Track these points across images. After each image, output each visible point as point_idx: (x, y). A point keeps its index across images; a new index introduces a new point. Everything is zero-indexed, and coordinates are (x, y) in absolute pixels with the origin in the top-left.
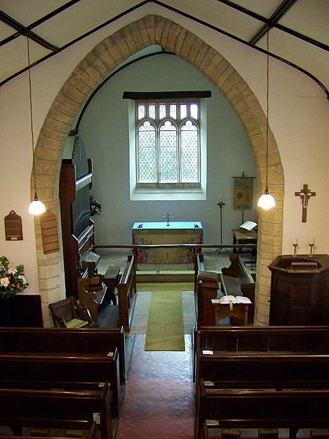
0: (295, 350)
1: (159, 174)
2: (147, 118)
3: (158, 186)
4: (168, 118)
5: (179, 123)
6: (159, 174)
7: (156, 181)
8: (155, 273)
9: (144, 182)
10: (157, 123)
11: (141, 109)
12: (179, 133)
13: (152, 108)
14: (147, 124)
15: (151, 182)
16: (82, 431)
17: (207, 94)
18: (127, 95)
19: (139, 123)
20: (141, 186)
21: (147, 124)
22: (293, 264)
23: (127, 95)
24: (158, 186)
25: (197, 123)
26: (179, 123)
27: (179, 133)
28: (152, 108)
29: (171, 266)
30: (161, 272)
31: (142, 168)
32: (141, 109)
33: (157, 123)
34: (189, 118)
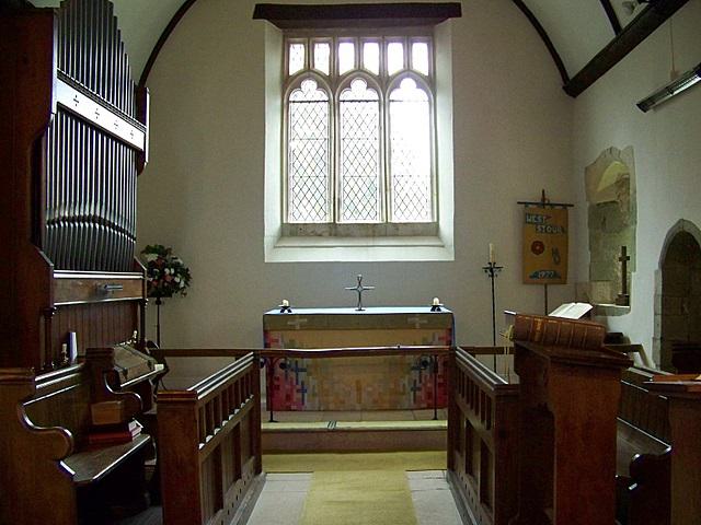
1: (336, 203)
2: (309, 71)
3: (336, 231)
7: (328, 219)
10: (334, 83)
11: (297, 53)
17: (454, 11)
19: (289, 83)
20: (291, 232)
23: (262, 12)
24: (336, 231)
25: (429, 83)
26: (383, 84)
33: (334, 83)
34: (408, 71)
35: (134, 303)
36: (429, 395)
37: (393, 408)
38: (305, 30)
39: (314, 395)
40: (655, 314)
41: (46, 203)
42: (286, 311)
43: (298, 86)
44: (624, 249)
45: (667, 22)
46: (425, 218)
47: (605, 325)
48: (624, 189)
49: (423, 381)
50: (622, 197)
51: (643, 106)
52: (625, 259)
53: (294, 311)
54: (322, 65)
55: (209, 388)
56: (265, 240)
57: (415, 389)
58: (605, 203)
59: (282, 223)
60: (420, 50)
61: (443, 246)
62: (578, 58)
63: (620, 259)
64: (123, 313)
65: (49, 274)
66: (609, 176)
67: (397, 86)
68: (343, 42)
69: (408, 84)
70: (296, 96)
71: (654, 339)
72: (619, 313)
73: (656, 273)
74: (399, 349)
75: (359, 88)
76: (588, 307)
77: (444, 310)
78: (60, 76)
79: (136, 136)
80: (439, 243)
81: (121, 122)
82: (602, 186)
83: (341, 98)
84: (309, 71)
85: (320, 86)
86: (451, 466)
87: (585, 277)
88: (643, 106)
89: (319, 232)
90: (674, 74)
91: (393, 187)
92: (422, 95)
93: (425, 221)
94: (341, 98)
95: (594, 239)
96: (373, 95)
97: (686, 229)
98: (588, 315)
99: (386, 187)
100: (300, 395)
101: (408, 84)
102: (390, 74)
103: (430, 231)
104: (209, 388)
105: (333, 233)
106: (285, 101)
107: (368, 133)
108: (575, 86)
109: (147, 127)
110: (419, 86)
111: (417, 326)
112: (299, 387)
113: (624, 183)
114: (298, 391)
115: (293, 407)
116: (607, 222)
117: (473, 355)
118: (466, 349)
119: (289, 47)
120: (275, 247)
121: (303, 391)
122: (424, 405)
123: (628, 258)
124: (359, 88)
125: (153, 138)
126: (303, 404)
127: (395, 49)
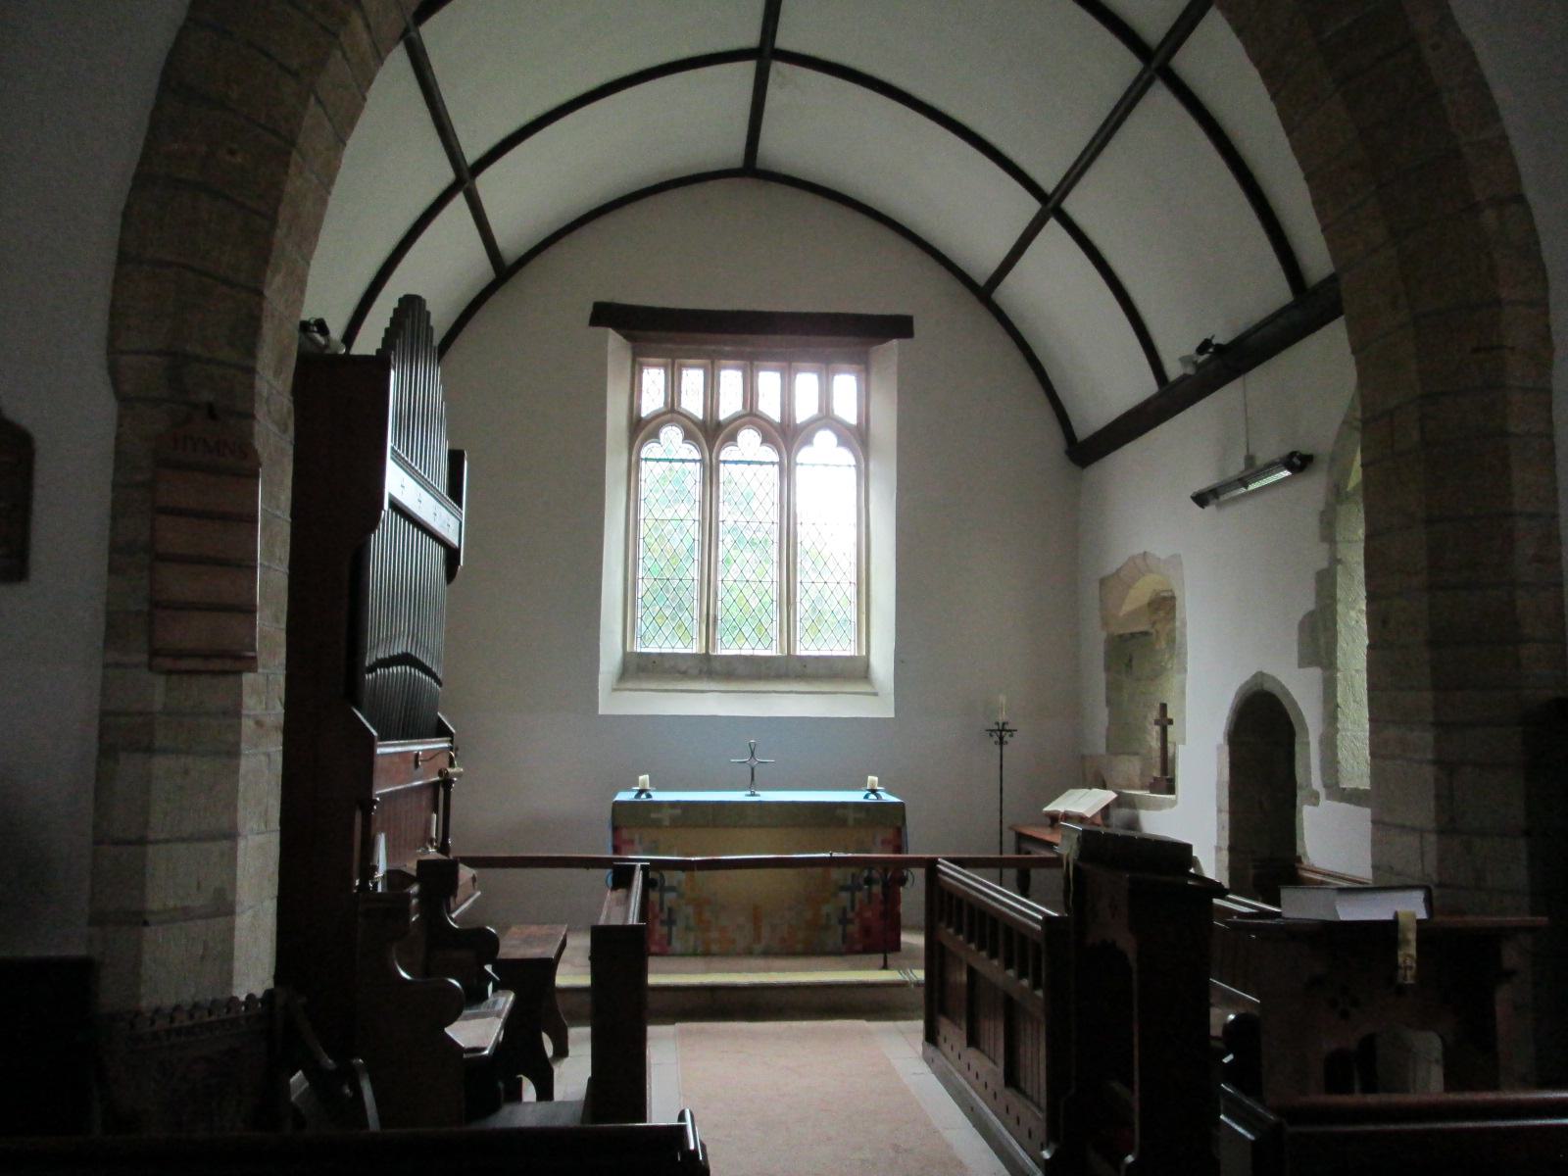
0: (1244, 997)
1: (710, 622)
2: (672, 412)
3: (709, 668)
4: (750, 415)
5: (785, 436)
6: (710, 622)
7: (696, 648)
8: (828, 855)
9: (653, 649)
10: (710, 433)
11: (653, 379)
12: (786, 471)
13: (408, 668)
14: (672, 435)
15: (680, 649)
16: (1343, 918)
17: (899, 327)
18: (606, 315)
19: (641, 429)
20: (642, 668)
21: (672, 435)
22: (1040, 917)
23: (606, 315)
24: (709, 668)
25: (858, 438)
26: (785, 436)
27: (786, 471)
28: (693, 379)
29: (716, 962)
30: (835, 855)
31: (649, 598)
32: (653, 379)
33: (710, 433)
34: (825, 417)
35: (435, 785)
36: (866, 931)
37: (811, 949)
38: (669, 346)
39: (688, 929)
40: (1219, 811)
41: (371, 638)
42: (643, 796)
43: (654, 435)
44: (1164, 707)
45: (1238, 382)
46: (842, 646)
47: (1133, 823)
48: (1162, 614)
49: (857, 907)
50: (1158, 626)
51: (1201, 499)
52: (1164, 722)
53: (658, 796)
54: (692, 402)
55: (981, 883)
56: (600, 677)
57: (844, 921)
58: (1133, 635)
59: (625, 653)
60: (846, 387)
61: (875, 694)
62: (1094, 412)
63: (1157, 723)
64: (425, 800)
65: (370, 744)
66: (1140, 594)
67: (808, 441)
68: (725, 368)
69: (825, 439)
70: (650, 450)
71: (1218, 849)
72: (1159, 806)
73: (1219, 748)
74: (831, 858)
75: (749, 440)
76: (1109, 796)
77: (887, 798)
78: (397, 458)
79: (445, 521)
80: (868, 689)
81: (426, 497)
82: (1127, 607)
83: (722, 458)
84: (672, 412)
85: (689, 437)
86: (931, 1037)
87: (1100, 746)
88: (1201, 499)
89: (684, 668)
90: (1250, 459)
91: (798, 599)
92: (846, 457)
93: (847, 654)
94: (722, 458)
95: (1113, 688)
96: (769, 454)
97: (1268, 686)
98: (1106, 811)
99: (788, 599)
100: (665, 930)
101: (825, 439)
102: (798, 421)
103: (850, 672)
104: (981, 883)
105: (705, 669)
106: (634, 459)
107: (760, 515)
108: (1087, 450)
109: (464, 512)
110: (843, 441)
111: (851, 822)
112: (665, 916)
113: (1164, 605)
114: (662, 922)
115: (714, 948)
116: (1134, 663)
117: (963, 867)
118: (961, 862)
119: (641, 372)
120: (614, 690)
121: (670, 922)
122: (859, 947)
123: (1171, 722)
124: (749, 440)
125: (473, 527)
126: (669, 942)
127: (807, 383)
